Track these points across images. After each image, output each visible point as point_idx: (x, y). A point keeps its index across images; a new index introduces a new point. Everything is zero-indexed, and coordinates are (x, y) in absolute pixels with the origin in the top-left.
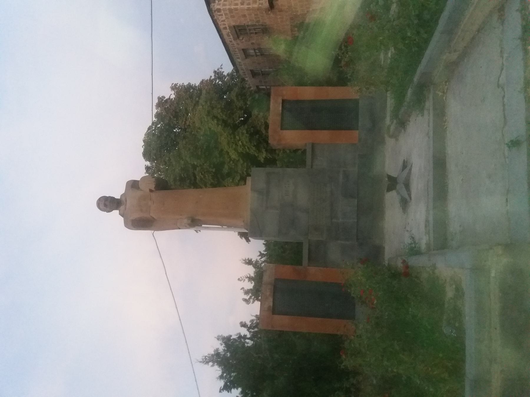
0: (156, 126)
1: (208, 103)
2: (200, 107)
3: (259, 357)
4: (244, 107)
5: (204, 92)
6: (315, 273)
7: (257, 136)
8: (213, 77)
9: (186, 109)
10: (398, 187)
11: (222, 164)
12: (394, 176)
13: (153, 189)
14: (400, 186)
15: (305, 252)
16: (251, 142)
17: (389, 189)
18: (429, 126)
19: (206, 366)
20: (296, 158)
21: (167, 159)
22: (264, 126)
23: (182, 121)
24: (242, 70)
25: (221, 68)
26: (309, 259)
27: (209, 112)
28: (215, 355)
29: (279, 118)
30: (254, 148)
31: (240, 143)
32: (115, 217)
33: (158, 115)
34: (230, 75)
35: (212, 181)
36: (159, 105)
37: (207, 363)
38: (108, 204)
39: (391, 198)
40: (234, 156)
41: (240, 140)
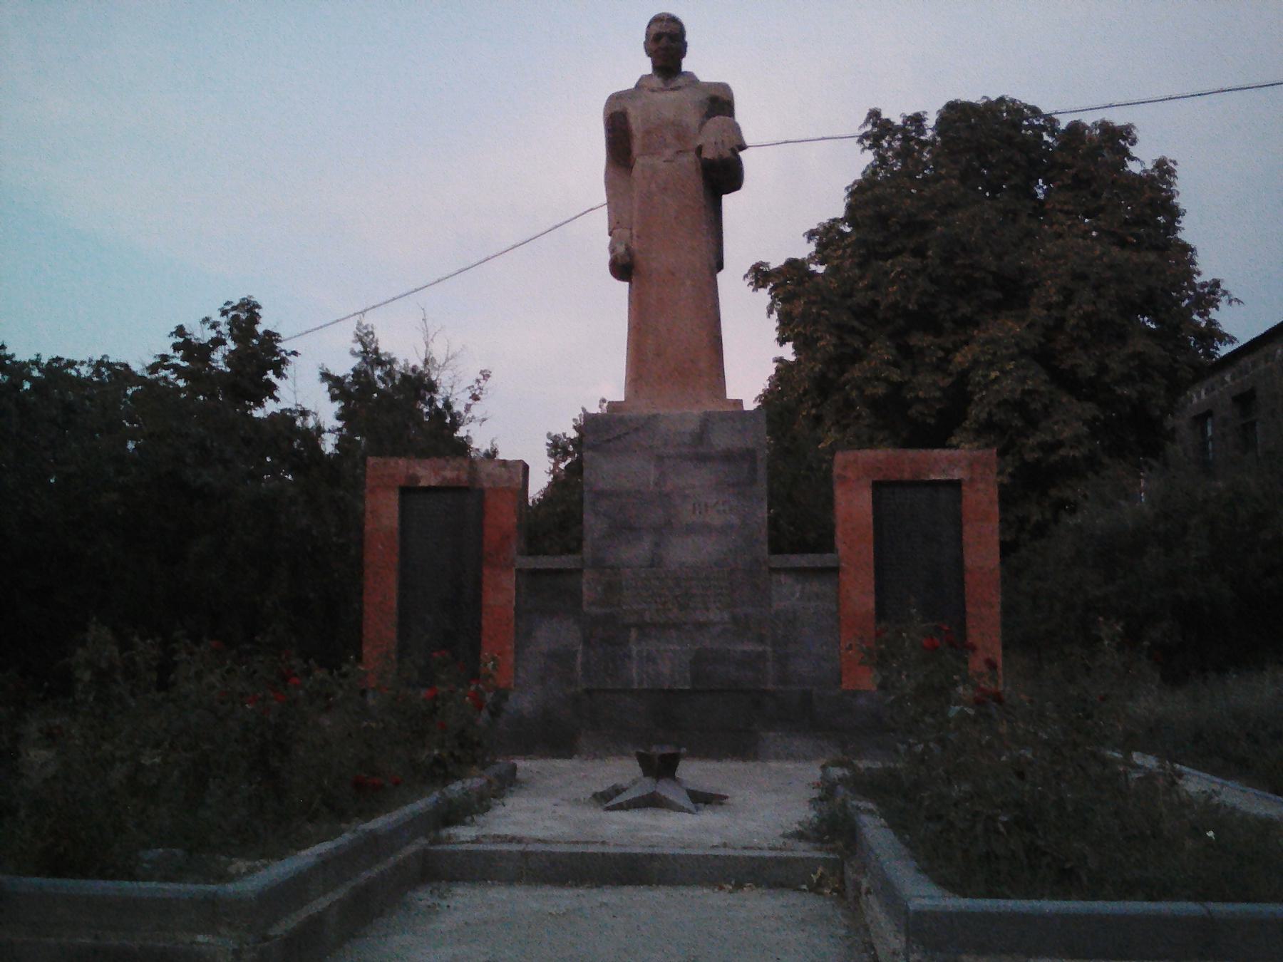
0: (1043, 128)
6: (501, 592)
7: (1018, 423)
9: (1102, 209)
10: (648, 780)
14: (647, 785)
15: (544, 562)
16: (999, 405)
18: (745, 848)
19: (352, 337)
22: (1049, 438)
24: (1254, 365)
25: (1230, 302)
26: (534, 573)
27: (1083, 277)
29: (907, 476)
30: (984, 416)
31: (993, 375)
33: (1076, 129)
34: (1212, 334)
36: (1106, 128)
37: (360, 339)
38: (667, 42)
39: (622, 771)
40: (961, 359)
41: (1003, 372)
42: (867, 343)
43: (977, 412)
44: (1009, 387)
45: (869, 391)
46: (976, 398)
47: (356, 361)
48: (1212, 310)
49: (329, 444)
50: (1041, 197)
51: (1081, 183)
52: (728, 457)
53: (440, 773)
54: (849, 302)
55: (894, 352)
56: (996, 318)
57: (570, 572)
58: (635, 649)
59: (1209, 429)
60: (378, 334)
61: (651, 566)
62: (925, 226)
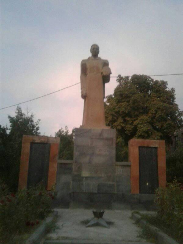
1: (164, 108)
2: (162, 104)
3: (16, 137)
4: (163, 128)
5: (171, 106)
6: (54, 167)
7: (146, 135)
8: (179, 111)
9: (161, 96)
10: (96, 219)
11: (131, 117)
12: (104, 216)
13: (103, 74)
14: (96, 220)
15: (63, 161)
17: (95, 213)
18: (129, 241)
19: (16, 109)
20: (122, 156)
21: (133, 87)
23: (154, 95)
26: (61, 164)
27: (159, 108)
28: (22, 114)
29: (146, 145)
30: (140, 134)
31: (142, 126)
32: (88, 55)
35: (121, 111)
37: (17, 110)
38: (95, 50)
39: (88, 214)
40: (136, 123)
42: (117, 118)
43: (138, 133)
44: (145, 129)
45: (118, 128)
46: (138, 130)
47: (16, 114)
48: (182, 116)
49: (8, 132)
50: (149, 94)
51: (157, 91)
52: (107, 139)
53: (42, 216)
54: (114, 110)
55: (123, 120)
56: (142, 115)
57: (70, 164)
58: (84, 183)
59: (177, 139)
60: (22, 109)
61: (89, 163)
62: (130, 97)
